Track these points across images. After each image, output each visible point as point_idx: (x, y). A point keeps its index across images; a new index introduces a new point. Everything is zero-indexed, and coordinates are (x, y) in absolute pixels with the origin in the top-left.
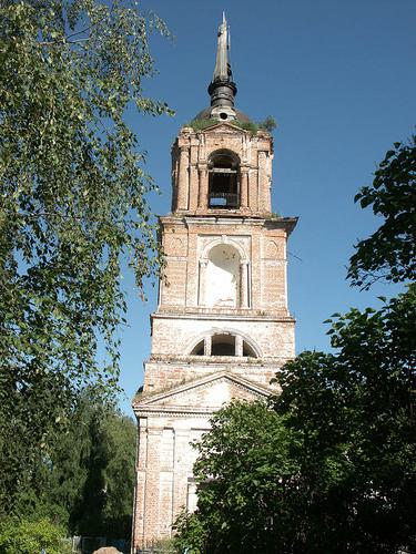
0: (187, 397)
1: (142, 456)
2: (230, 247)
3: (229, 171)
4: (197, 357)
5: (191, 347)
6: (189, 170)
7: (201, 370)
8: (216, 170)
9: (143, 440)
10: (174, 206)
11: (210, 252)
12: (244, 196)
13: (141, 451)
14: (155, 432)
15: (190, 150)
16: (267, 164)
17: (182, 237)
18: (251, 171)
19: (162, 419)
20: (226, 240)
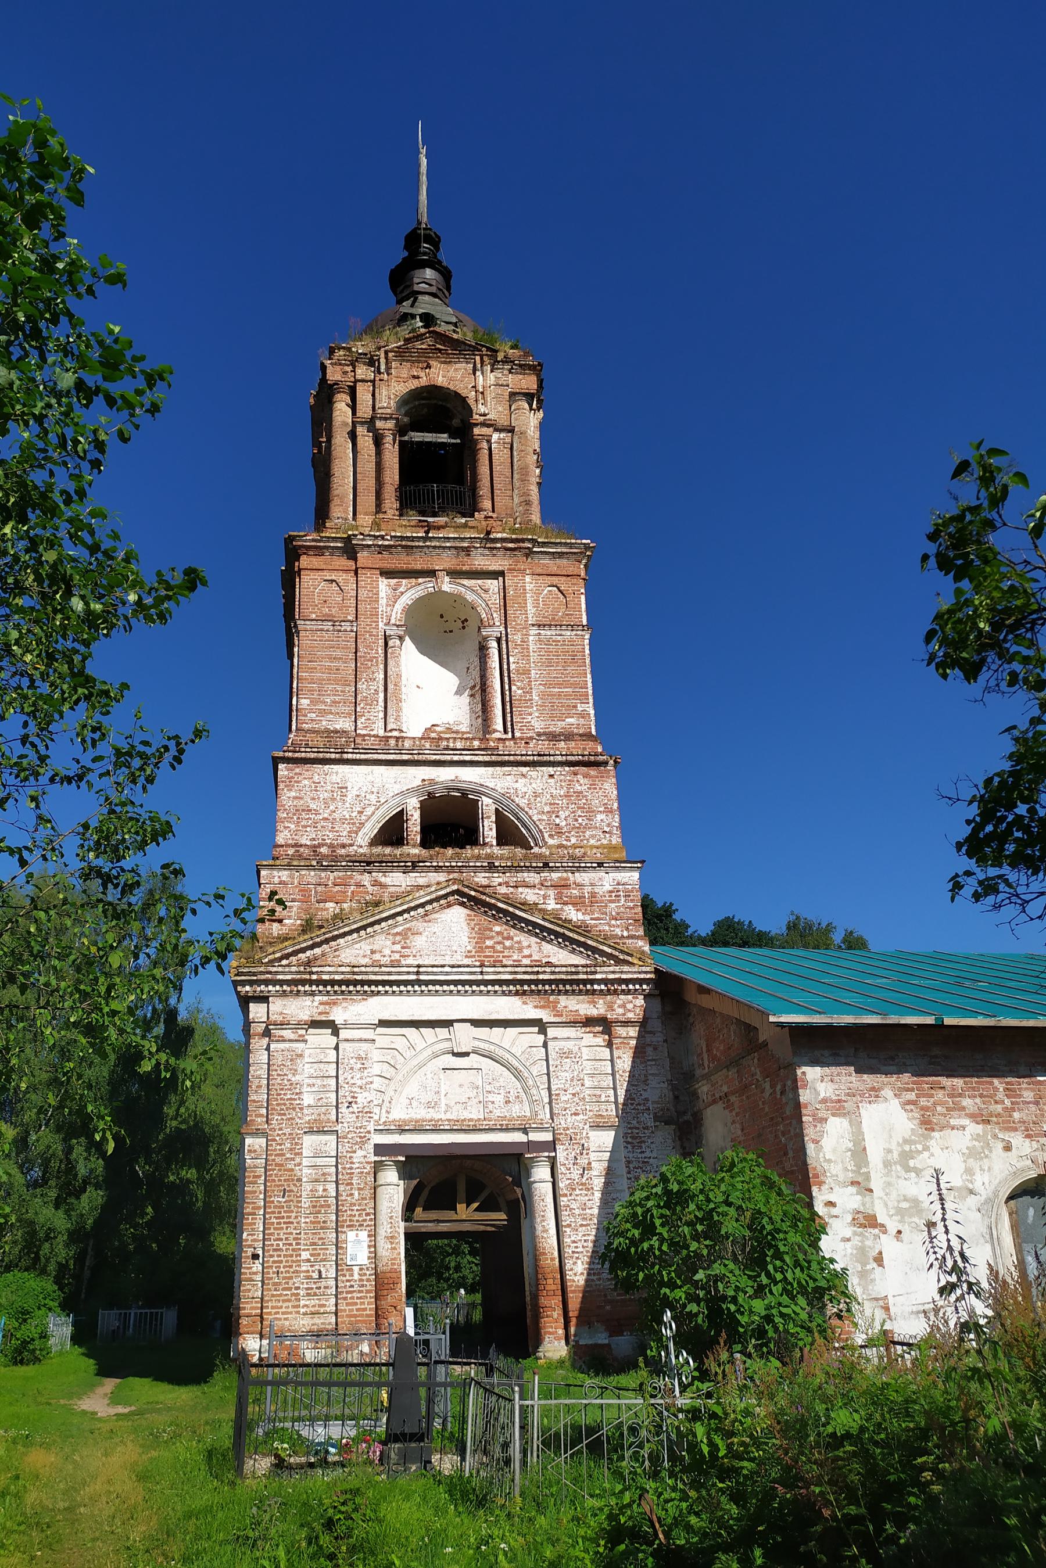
0: (365, 947)
1: (257, 1096)
2: (457, 599)
3: (443, 438)
4: (388, 850)
5: (371, 829)
6: (353, 436)
7: (397, 880)
8: (417, 436)
9: (259, 1057)
10: (322, 514)
11: (410, 611)
12: (484, 491)
13: (254, 1084)
14: (287, 1034)
15: (353, 392)
16: (530, 421)
17: (341, 577)
18: (495, 436)
19: (307, 1001)
20: (447, 585)
